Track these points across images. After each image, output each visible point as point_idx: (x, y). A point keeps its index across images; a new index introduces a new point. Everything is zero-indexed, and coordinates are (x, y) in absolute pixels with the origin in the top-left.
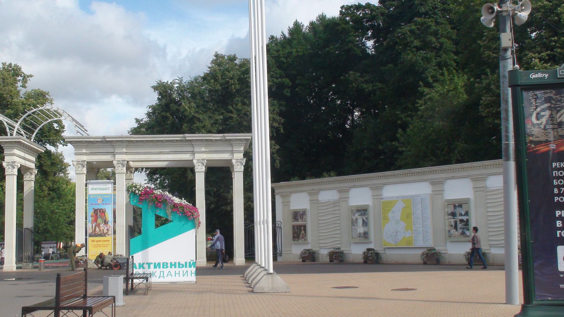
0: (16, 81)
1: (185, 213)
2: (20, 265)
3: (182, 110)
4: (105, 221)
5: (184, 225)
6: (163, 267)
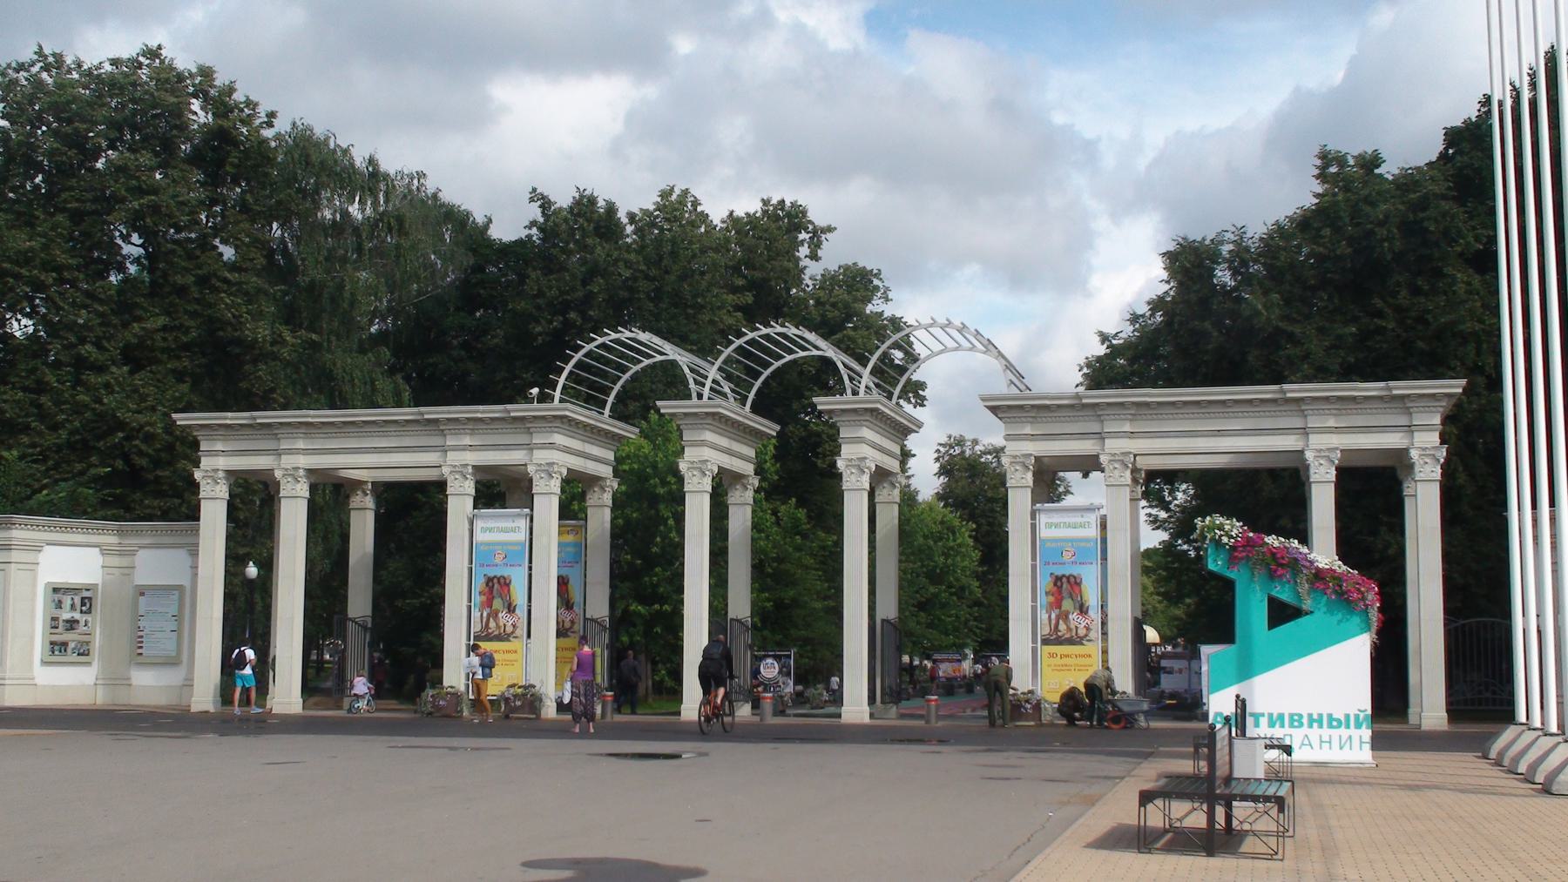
0: (797, 244)
1: (1342, 594)
3: (1247, 313)
5: (1340, 622)
6: (1291, 726)
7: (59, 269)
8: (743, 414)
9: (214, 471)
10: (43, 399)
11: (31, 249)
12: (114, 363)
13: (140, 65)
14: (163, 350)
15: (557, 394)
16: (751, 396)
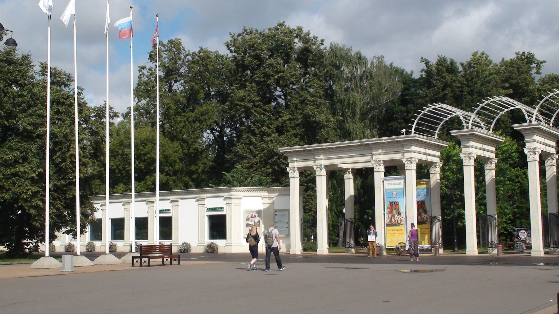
0: (530, 69)
2: (547, 250)
4: (399, 212)
7: (254, 102)
8: (490, 134)
9: (294, 167)
10: (251, 147)
11: (244, 96)
12: (273, 133)
13: (278, 29)
14: (291, 127)
15: (413, 131)
16: (552, 120)
